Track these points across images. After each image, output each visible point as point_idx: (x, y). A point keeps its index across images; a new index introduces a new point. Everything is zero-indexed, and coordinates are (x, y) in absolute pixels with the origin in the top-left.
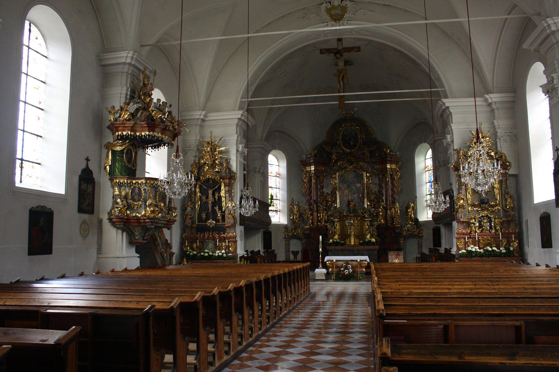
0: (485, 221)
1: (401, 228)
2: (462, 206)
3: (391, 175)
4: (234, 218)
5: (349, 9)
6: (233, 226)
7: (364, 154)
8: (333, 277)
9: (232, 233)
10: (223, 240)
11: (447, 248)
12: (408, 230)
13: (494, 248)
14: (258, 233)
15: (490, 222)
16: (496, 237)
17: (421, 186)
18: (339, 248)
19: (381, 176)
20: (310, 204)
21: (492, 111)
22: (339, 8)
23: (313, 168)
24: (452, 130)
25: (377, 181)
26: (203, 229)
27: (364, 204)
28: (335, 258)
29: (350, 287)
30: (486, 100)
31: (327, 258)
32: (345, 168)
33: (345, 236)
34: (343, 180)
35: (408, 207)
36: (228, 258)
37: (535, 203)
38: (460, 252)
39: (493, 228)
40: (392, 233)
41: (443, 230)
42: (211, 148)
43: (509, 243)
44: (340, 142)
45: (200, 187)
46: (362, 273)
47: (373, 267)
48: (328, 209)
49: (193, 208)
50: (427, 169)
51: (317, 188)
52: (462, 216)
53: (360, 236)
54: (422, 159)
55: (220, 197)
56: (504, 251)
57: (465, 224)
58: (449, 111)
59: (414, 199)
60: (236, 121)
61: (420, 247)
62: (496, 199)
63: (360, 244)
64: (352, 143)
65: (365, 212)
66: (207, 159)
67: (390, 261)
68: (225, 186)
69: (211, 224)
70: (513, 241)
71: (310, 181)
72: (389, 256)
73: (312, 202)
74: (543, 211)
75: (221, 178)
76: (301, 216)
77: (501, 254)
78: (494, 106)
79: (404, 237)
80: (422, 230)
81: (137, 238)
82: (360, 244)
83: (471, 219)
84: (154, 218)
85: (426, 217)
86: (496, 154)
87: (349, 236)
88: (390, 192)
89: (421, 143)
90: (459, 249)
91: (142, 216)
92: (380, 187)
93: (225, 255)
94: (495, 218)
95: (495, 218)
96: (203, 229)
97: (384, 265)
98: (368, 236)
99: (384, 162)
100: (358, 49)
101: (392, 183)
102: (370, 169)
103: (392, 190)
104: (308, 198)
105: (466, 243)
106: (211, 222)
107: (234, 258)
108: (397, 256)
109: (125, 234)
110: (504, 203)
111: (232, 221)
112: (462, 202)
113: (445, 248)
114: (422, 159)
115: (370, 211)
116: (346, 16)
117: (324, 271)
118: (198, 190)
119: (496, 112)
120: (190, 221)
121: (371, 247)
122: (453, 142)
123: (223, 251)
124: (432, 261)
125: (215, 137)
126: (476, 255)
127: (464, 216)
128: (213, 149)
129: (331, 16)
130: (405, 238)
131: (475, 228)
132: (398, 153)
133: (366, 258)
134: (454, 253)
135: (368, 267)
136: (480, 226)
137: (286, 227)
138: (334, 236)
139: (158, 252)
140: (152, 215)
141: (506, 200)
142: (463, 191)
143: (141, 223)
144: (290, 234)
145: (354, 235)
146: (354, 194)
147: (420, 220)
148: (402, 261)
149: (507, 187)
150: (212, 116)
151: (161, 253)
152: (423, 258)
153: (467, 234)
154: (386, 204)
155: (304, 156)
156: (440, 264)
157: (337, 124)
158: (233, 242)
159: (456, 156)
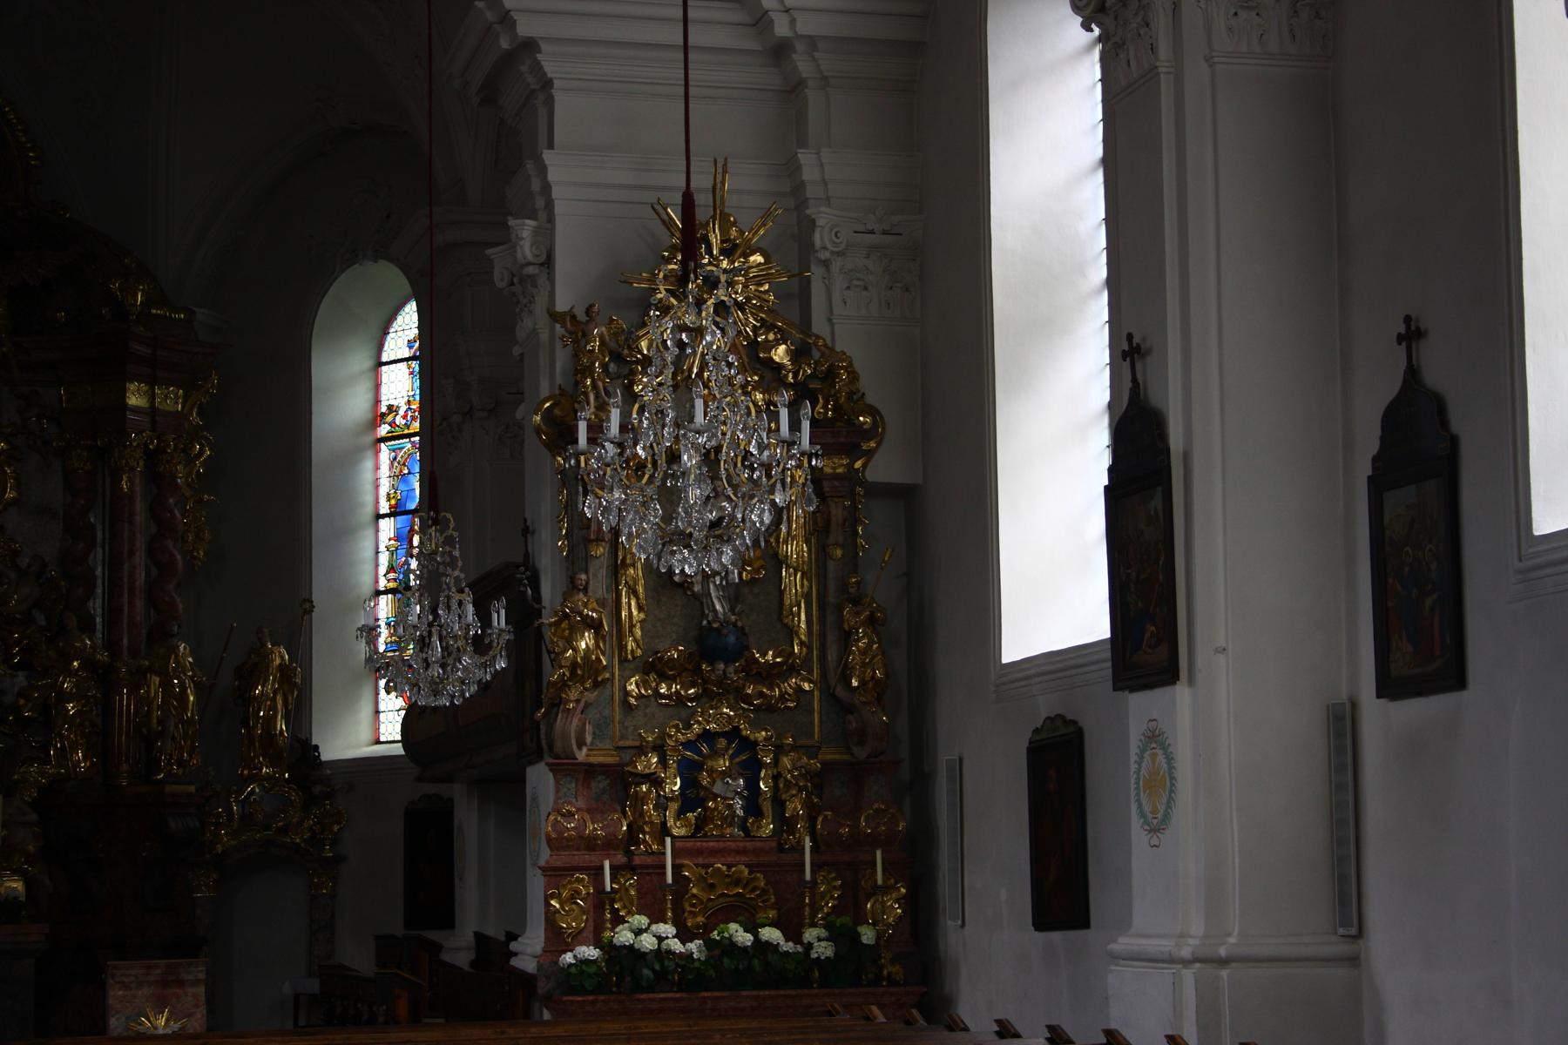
0: (723, 764)
2: (588, 670)
3: (152, 457)
13: (771, 934)
15: (751, 769)
17: (345, 532)
21: (793, 91)
24: (546, 188)
35: (253, 669)
37: (1005, 660)
38: (568, 958)
39: (767, 807)
41: (469, 820)
50: (384, 430)
52: (583, 731)
54: (359, 361)
56: (823, 950)
57: (601, 783)
58: (537, 68)
62: (791, 632)
67: (115, 1024)
70: (876, 891)
72: (115, 994)
74: (1045, 707)
77: (804, 970)
78: (802, 64)
83: (641, 750)
85: (365, 733)
86: (797, 355)
88: (139, 568)
89: (353, 258)
90: (558, 940)
94: (779, 750)
95: (779, 750)
105: (601, 900)
110: (832, 655)
112: (585, 642)
114: (359, 361)
119: (813, 97)
122: (548, 263)
127: (600, 729)
131: (661, 806)
136: (692, 798)
141: (847, 637)
147: (327, 754)
149: (852, 562)
154: (111, 644)
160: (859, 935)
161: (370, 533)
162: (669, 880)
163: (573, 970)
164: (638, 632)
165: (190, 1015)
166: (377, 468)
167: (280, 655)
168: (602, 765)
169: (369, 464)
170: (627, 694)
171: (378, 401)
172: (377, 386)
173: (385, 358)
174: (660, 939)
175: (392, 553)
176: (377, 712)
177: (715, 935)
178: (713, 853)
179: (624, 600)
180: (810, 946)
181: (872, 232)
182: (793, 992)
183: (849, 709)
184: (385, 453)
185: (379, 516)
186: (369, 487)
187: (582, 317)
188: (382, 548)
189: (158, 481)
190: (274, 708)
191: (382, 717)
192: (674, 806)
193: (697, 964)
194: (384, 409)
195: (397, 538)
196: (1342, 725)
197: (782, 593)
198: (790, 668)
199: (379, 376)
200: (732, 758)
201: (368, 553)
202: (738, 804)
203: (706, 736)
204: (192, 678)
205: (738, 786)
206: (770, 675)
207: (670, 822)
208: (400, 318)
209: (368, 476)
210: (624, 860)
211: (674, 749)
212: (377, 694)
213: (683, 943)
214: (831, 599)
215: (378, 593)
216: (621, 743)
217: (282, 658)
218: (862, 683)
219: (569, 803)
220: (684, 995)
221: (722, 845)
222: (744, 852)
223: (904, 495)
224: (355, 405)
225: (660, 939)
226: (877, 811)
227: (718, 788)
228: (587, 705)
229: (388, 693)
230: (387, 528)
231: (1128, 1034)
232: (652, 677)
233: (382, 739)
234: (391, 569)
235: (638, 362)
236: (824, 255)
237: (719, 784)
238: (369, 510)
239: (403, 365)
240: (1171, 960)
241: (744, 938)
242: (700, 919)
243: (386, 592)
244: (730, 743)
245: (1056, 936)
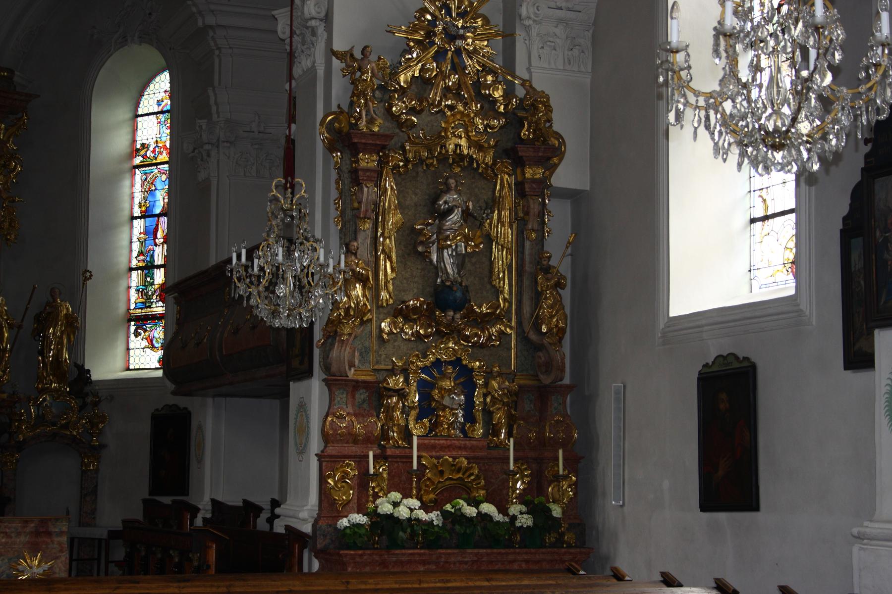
0: (447, 384)
11: (220, 498)
13: (488, 508)
15: (468, 387)
17: (110, 227)
37: (675, 310)
38: (344, 522)
39: (479, 416)
50: (138, 160)
54: (123, 113)
56: (525, 521)
57: (362, 395)
62: (498, 291)
70: (557, 478)
80: (103, 419)
83: (392, 372)
85: (120, 363)
86: (508, 94)
89: (124, 41)
90: (329, 506)
94: (489, 376)
95: (489, 376)
105: (364, 478)
110: (527, 309)
113: (214, 502)
114: (123, 113)
131: (405, 411)
136: (427, 409)
141: (537, 298)
142: (362, 244)
147: (96, 376)
153: (368, 440)
160: (550, 510)
161: (126, 229)
162: (415, 467)
163: (348, 531)
164: (391, 287)
165: (57, 558)
166: (133, 185)
167: (67, 308)
168: (365, 382)
169: (127, 183)
170: (381, 331)
171: (134, 141)
172: (134, 131)
173: (140, 112)
174: (411, 510)
175: (142, 242)
176: (128, 349)
177: (448, 507)
178: (443, 448)
179: (382, 263)
180: (514, 518)
181: (561, 9)
182: (503, 551)
183: (539, 347)
184: (138, 176)
185: (133, 218)
186: (127, 198)
187: (358, 55)
188: (135, 239)
190: (62, 343)
191: (132, 352)
192: (413, 413)
193: (436, 529)
194: (138, 146)
195: (146, 233)
197: (491, 263)
199: (143, 121)
200: (455, 379)
201: (125, 242)
202: (460, 413)
203: (438, 363)
204: (6, 320)
205: (460, 400)
207: (411, 425)
208: (152, 86)
209: (126, 190)
210: (378, 451)
211: (415, 372)
212: (129, 337)
213: (427, 513)
214: (528, 268)
215: (131, 269)
216: (376, 367)
217: (68, 309)
218: (550, 330)
219: (342, 409)
220: (427, 551)
221: (449, 442)
222: (465, 448)
224: (119, 143)
225: (411, 510)
226: (558, 421)
227: (446, 401)
228: (356, 337)
229: (136, 336)
230: (139, 226)
231: (794, 587)
232: (400, 319)
233: (131, 367)
234: (141, 253)
235: (396, 91)
236: (527, 23)
237: (447, 399)
238: (126, 213)
239: (153, 117)
242: (432, 496)
243: (137, 269)
244: (454, 369)
245: (723, 517)
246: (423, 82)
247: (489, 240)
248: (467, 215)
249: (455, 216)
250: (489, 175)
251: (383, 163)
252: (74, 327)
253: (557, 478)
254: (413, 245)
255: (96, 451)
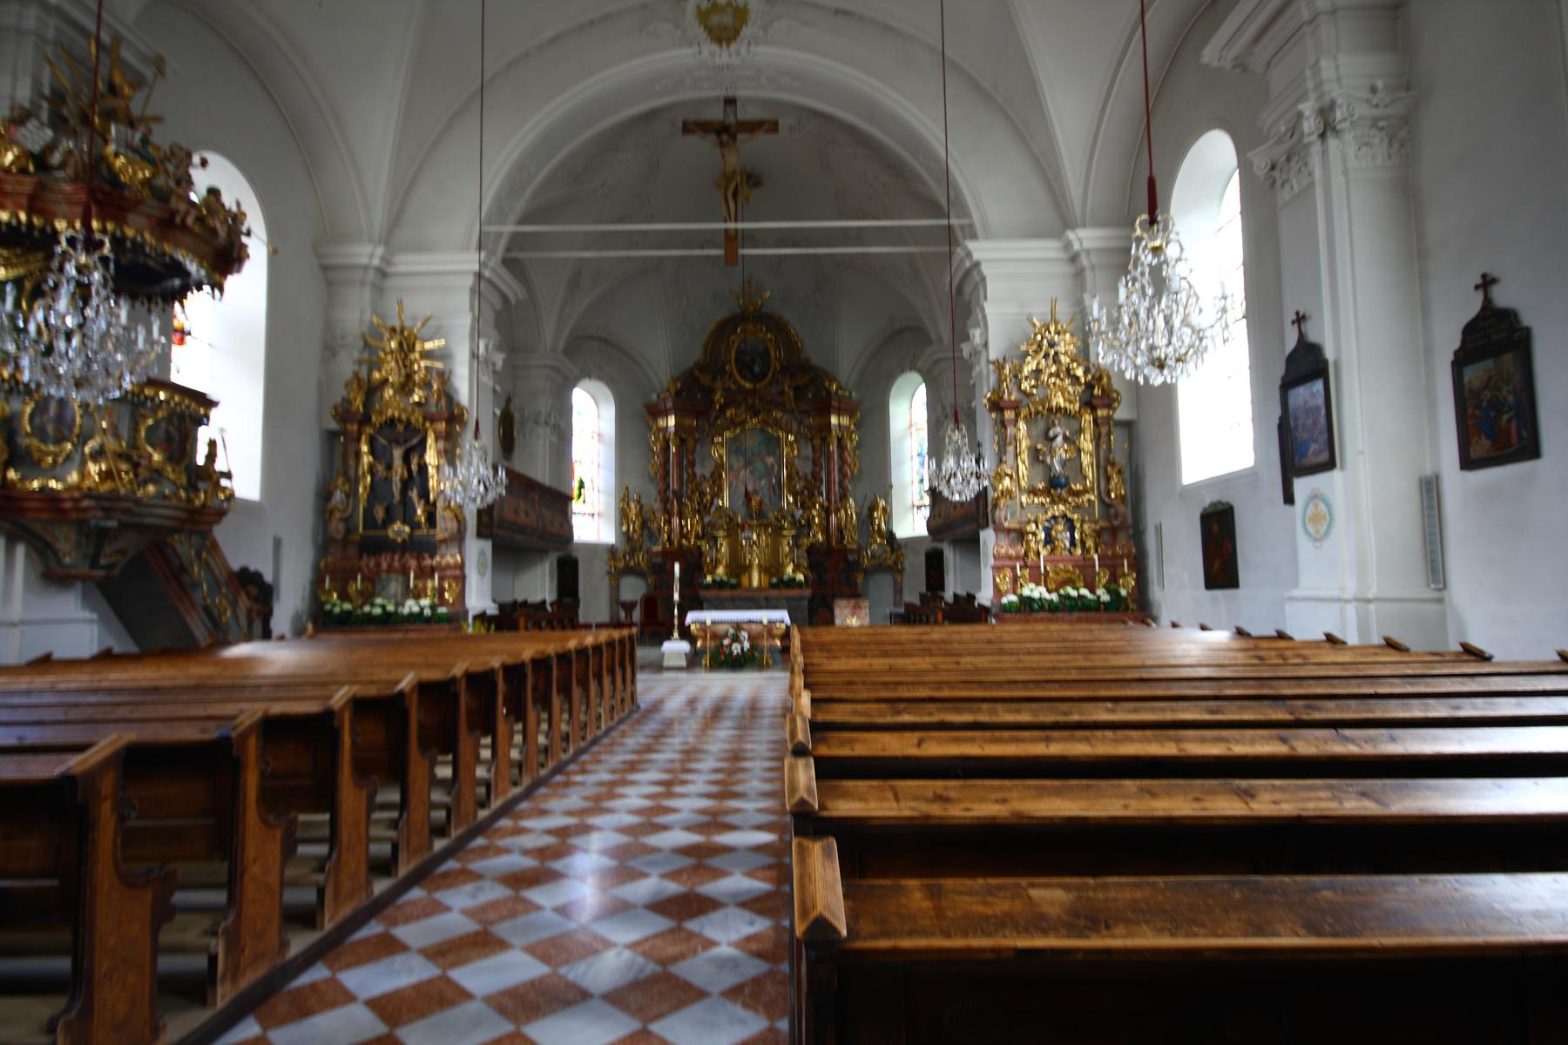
0: (1060, 527)
1: (859, 551)
2: (1008, 493)
3: (840, 440)
4: (460, 520)
5: (752, 16)
6: (458, 538)
7: (782, 393)
8: (706, 660)
9: (453, 556)
10: (425, 573)
12: (873, 556)
13: (1084, 592)
14: (542, 560)
15: (1072, 529)
16: (1085, 567)
18: (727, 593)
19: (817, 442)
20: (665, 501)
21: (1079, 275)
22: (730, 11)
23: (672, 421)
24: (984, 317)
25: (809, 451)
26: (376, 546)
27: (780, 498)
28: (709, 616)
29: (743, 685)
30: (1068, 246)
31: (691, 617)
32: (743, 423)
33: (738, 568)
34: (735, 447)
35: (873, 507)
36: (434, 619)
40: (837, 568)
41: (950, 556)
42: (400, 344)
43: (1114, 579)
44: (732, 367)
45: (372, 443)
46: (772, 649)
47: (795, 633)
48: (703, 509)
49: (352, 494)
51: (680, 465)
52: (1007, 516)
53: (772, 568)
55: (423, 468)
56: (1105, 598)
57: (1013, 535)
58: (980, 272)
59: (886, 490)
60: (469, 281)
61: (898, 590)
62: (1085, 478)
63: (772, 586)
64: (757, 369)
65: (784, 518)
66: (390, 370)
67: (838, 622)
68: (437, 439)
69: (398, 533)
70: (1124, 575)
71: (666, 449)
72: (837, 612)
73: (670, 495)
74: (1208, 499)
75: (425, 419)
76: (644, 525)
77: (1097, 606)
78: (1084, 261)
79: (865, 571)
81: (67, 560)
82: (772, 586)
83: (1029, 522)
84: (113, 496)
86: (1086, 372)
87: (747, 569)
88: (836, 475)
89: (903, 371)
90: (998, 592)
91: (69, 488)
92: (816, 463)
93: (427, 612)
96: (376, 546)
97: (826, 635)
98: (789, 569)
99: (825, 409)
100: (774, 127)
101: (841, 457)
102: (795, 426)
103: (840, 470)
104: (662, 485)
105: (1015, 579)
106: (399, 530)
107: (456, 617)
108: (855, 610)
109: (20, 551)
111: (452, 526)
112: (1007, 481)
115: (793, 516)
116: (746, 31)
117: (685, 646)
118: (365, 448)
119: (1089, 275)
120: (341, 526)
121: (795, 592)
122: (986, 345)
123: (425, 602)
124: (936, 623)
125: (414, 319)
126: (1042, 608)
127: (1013, 515)
128: (407, 347)
129: (710, 30)
130: (868, 573)
131: (1037, 542)
132: (854, 394)
133: (782, 616)
134: (987, 603)
135: (786, 636)
136: (1049, 540)
137: (612, 550)
138: (716, 567)
139: (193, 605)
140: (106, 487)
141: (1108, 479)
142: (1009, 457)
143: (63, 512)
144: (621, 565)
145: (760, 565)
146: (760, 478)
148: (867, 621)
149: (1109, 450)
150: (406, 263)
151: (207, 610)
152: (910, 617)
153: (1017, 558)
154: (828, 499)
155: (654, 397)
156: (1017, 627)
157: (724, 329)
158: (455, 578)
159: (993, 379)
189: (841, 446)
196: (1430, 489)
198: (1085, 491)
203: (1054, 517)
206: (1077, 494)
223: (1128, 425)
240: (1339, 600)
241: (1074, 593)
245: (1218, 593)
246: (1037, 372)
247: (1079, 451)
248: (1065, 439)
249: (1060, 439)
250: (1076, 417)
251: (1017, 415)
252: (887, 513)
253: (1124, 575)
254: (1035, 454)
255: (901, 572)
